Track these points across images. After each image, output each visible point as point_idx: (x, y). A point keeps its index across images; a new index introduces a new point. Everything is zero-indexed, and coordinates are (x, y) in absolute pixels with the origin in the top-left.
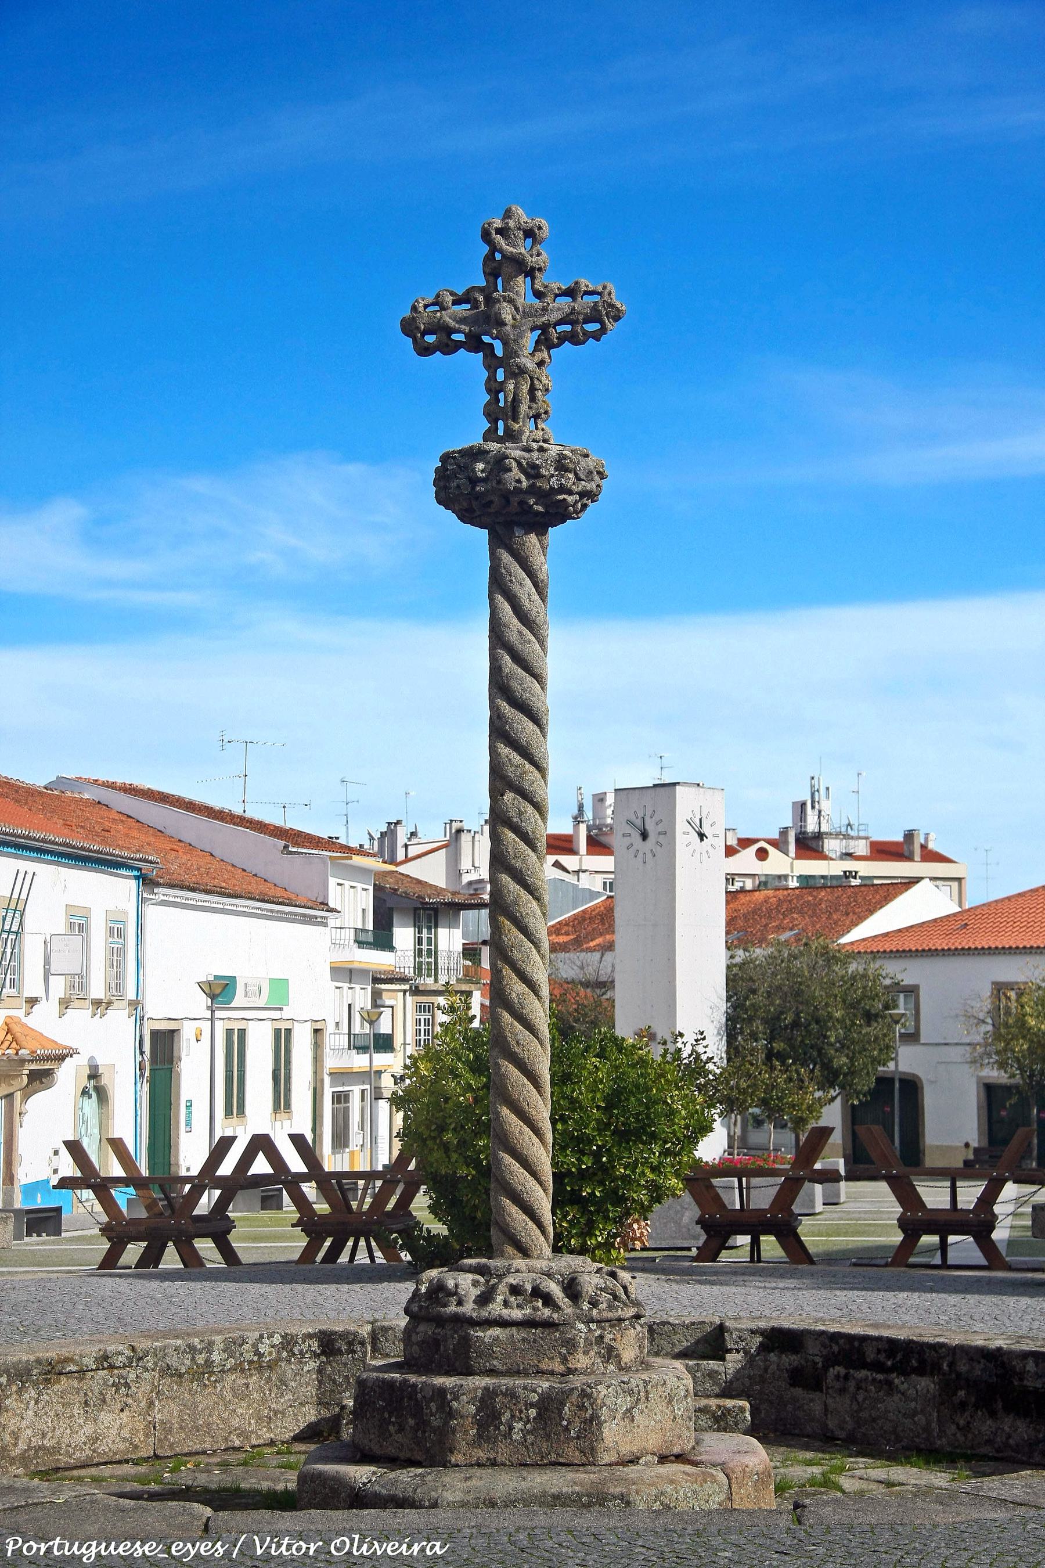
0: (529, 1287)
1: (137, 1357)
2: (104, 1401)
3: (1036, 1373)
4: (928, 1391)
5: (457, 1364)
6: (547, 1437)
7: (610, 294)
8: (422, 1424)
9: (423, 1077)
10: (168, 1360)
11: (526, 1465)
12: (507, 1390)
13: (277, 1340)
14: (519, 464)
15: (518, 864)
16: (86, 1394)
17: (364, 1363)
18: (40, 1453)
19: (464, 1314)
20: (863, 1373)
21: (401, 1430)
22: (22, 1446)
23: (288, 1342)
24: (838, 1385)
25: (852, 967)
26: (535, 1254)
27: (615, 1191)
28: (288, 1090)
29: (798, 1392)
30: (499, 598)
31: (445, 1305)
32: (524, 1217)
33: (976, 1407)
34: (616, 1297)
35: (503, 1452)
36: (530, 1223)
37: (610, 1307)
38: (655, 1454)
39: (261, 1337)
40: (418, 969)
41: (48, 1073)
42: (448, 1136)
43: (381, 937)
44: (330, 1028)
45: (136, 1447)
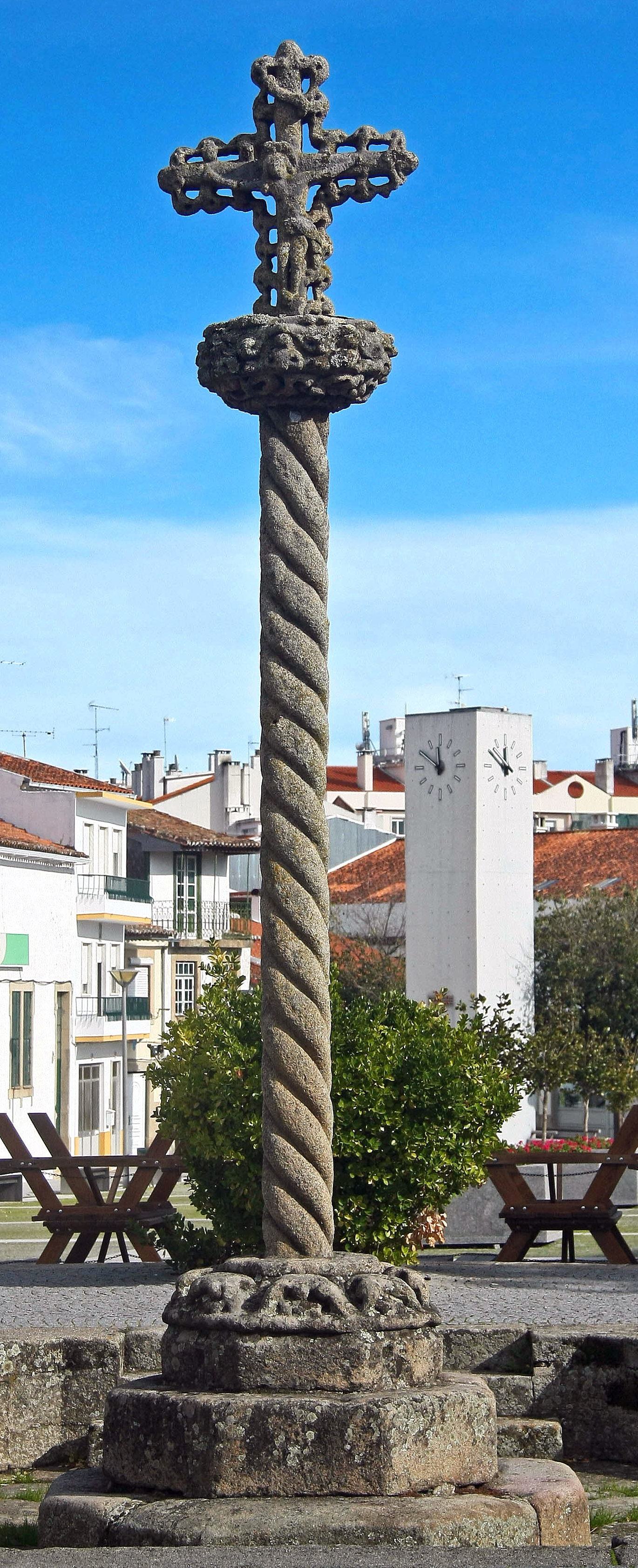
0: (306, 1290)
6: (328, 1464)
7: (400, 143)
8: (183, 1448)
12: (281, 1409)
14: (295, 339)
15: (294, 801)
17: (116, 1377)
19: (231, 1322)
21: (158, 1455)
23: (29, 1354)
28: (28, 1063)
30: (273, 495)
31: (209, 1311)
34: (406, 1302)
35: (277, 1480)
36: (308, 1216)
37: (400, 1314)
40: (179, 922)
42: (213, 1116)
43: (136, 887)
44: (77, 991)
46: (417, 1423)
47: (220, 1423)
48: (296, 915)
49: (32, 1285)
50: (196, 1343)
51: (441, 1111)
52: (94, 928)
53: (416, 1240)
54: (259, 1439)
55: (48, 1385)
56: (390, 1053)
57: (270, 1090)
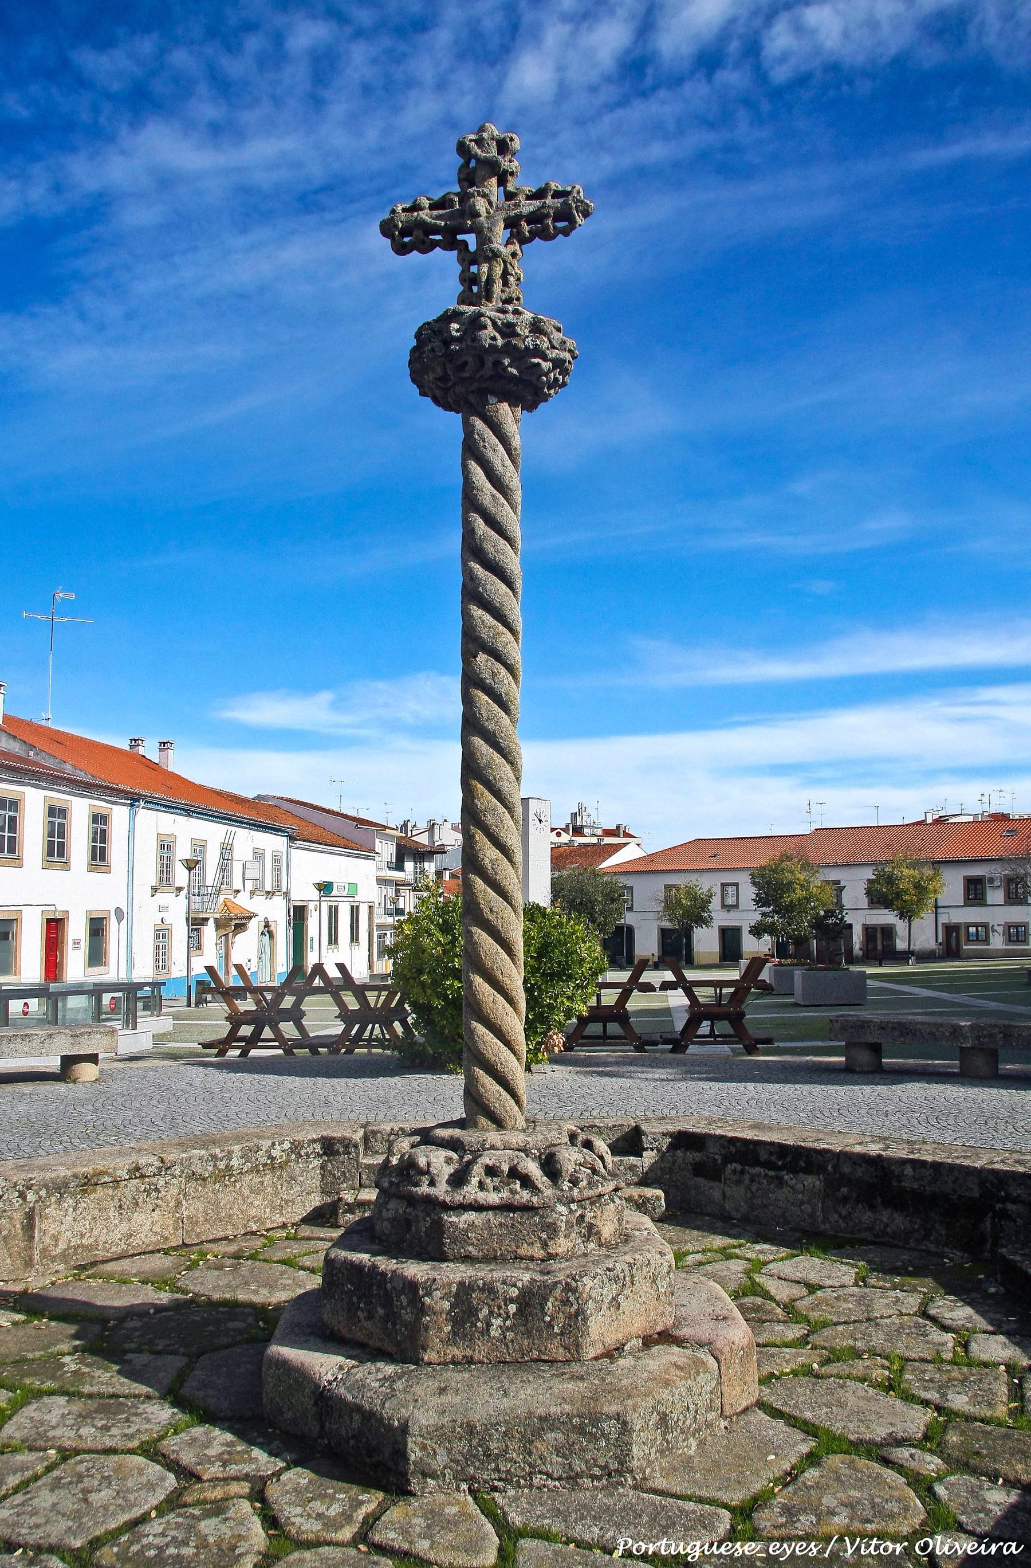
0: (505, 1168)
1: (165, 1167)
2: (137, 1204)
3: (913, 1177)
4: (814, 1187)
5: (430, 1248)
6: (528, 1334)
7: (578, 193)
8: (392, 1316)
9: (407, 935)
10: (193, 1168)
11: (505, 1362)
12: (484, 1284)
13: (287, 1145)
14: (494, 323)
15: (491, 726)
16: (120, 1200)
17: (357, 1161)
18: (80, 1251)
19: (437, 1198)
20: (757, 1170)
21: (370, 1317)
22: (62, 1246)
23: (296, 1148)
24: (734, 1178)
25: (605, 879)
26: (510, 1124)
27: (541, 1014)
28: (357, 933)
29: (700, 1180)
30: (473, 465)
31: (417, 1184)
32: (498, 1088)
33: (858, 1201)
34: (594, 1171)
35: (480, 1350)
36: (504, 1093)
37: (591, 1184)
38: (639, 1337)
39: (273, 1144)
41: (244, 925)
42: (424, 978)
43: (399, 866)
44: (377, 905)
45: (167, 1239)
46: (609, 1291)
47: (426, 1298)
48: (494, 827)
49: (315, 1076)
50: (404, 1212)
51: (565, 974)
52: (382, 882)
53: (547, 1049)
54: (464, 1312)
55: (311, 1166)
56: (533, 939)
57: (470, 983)
